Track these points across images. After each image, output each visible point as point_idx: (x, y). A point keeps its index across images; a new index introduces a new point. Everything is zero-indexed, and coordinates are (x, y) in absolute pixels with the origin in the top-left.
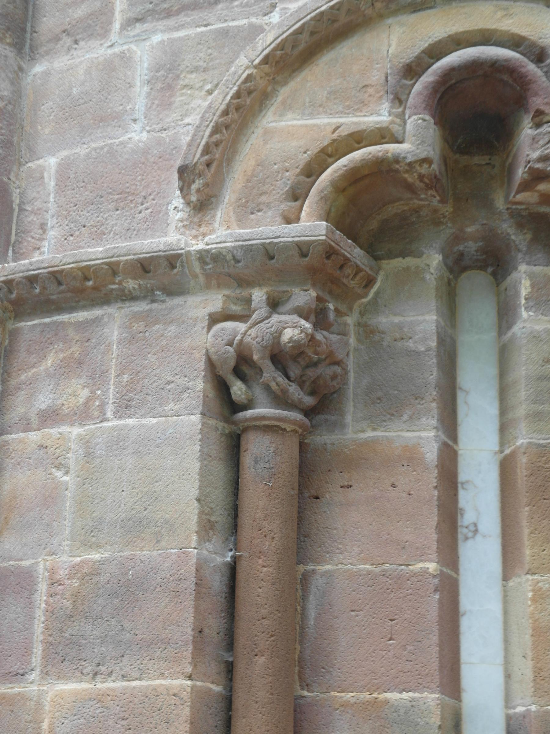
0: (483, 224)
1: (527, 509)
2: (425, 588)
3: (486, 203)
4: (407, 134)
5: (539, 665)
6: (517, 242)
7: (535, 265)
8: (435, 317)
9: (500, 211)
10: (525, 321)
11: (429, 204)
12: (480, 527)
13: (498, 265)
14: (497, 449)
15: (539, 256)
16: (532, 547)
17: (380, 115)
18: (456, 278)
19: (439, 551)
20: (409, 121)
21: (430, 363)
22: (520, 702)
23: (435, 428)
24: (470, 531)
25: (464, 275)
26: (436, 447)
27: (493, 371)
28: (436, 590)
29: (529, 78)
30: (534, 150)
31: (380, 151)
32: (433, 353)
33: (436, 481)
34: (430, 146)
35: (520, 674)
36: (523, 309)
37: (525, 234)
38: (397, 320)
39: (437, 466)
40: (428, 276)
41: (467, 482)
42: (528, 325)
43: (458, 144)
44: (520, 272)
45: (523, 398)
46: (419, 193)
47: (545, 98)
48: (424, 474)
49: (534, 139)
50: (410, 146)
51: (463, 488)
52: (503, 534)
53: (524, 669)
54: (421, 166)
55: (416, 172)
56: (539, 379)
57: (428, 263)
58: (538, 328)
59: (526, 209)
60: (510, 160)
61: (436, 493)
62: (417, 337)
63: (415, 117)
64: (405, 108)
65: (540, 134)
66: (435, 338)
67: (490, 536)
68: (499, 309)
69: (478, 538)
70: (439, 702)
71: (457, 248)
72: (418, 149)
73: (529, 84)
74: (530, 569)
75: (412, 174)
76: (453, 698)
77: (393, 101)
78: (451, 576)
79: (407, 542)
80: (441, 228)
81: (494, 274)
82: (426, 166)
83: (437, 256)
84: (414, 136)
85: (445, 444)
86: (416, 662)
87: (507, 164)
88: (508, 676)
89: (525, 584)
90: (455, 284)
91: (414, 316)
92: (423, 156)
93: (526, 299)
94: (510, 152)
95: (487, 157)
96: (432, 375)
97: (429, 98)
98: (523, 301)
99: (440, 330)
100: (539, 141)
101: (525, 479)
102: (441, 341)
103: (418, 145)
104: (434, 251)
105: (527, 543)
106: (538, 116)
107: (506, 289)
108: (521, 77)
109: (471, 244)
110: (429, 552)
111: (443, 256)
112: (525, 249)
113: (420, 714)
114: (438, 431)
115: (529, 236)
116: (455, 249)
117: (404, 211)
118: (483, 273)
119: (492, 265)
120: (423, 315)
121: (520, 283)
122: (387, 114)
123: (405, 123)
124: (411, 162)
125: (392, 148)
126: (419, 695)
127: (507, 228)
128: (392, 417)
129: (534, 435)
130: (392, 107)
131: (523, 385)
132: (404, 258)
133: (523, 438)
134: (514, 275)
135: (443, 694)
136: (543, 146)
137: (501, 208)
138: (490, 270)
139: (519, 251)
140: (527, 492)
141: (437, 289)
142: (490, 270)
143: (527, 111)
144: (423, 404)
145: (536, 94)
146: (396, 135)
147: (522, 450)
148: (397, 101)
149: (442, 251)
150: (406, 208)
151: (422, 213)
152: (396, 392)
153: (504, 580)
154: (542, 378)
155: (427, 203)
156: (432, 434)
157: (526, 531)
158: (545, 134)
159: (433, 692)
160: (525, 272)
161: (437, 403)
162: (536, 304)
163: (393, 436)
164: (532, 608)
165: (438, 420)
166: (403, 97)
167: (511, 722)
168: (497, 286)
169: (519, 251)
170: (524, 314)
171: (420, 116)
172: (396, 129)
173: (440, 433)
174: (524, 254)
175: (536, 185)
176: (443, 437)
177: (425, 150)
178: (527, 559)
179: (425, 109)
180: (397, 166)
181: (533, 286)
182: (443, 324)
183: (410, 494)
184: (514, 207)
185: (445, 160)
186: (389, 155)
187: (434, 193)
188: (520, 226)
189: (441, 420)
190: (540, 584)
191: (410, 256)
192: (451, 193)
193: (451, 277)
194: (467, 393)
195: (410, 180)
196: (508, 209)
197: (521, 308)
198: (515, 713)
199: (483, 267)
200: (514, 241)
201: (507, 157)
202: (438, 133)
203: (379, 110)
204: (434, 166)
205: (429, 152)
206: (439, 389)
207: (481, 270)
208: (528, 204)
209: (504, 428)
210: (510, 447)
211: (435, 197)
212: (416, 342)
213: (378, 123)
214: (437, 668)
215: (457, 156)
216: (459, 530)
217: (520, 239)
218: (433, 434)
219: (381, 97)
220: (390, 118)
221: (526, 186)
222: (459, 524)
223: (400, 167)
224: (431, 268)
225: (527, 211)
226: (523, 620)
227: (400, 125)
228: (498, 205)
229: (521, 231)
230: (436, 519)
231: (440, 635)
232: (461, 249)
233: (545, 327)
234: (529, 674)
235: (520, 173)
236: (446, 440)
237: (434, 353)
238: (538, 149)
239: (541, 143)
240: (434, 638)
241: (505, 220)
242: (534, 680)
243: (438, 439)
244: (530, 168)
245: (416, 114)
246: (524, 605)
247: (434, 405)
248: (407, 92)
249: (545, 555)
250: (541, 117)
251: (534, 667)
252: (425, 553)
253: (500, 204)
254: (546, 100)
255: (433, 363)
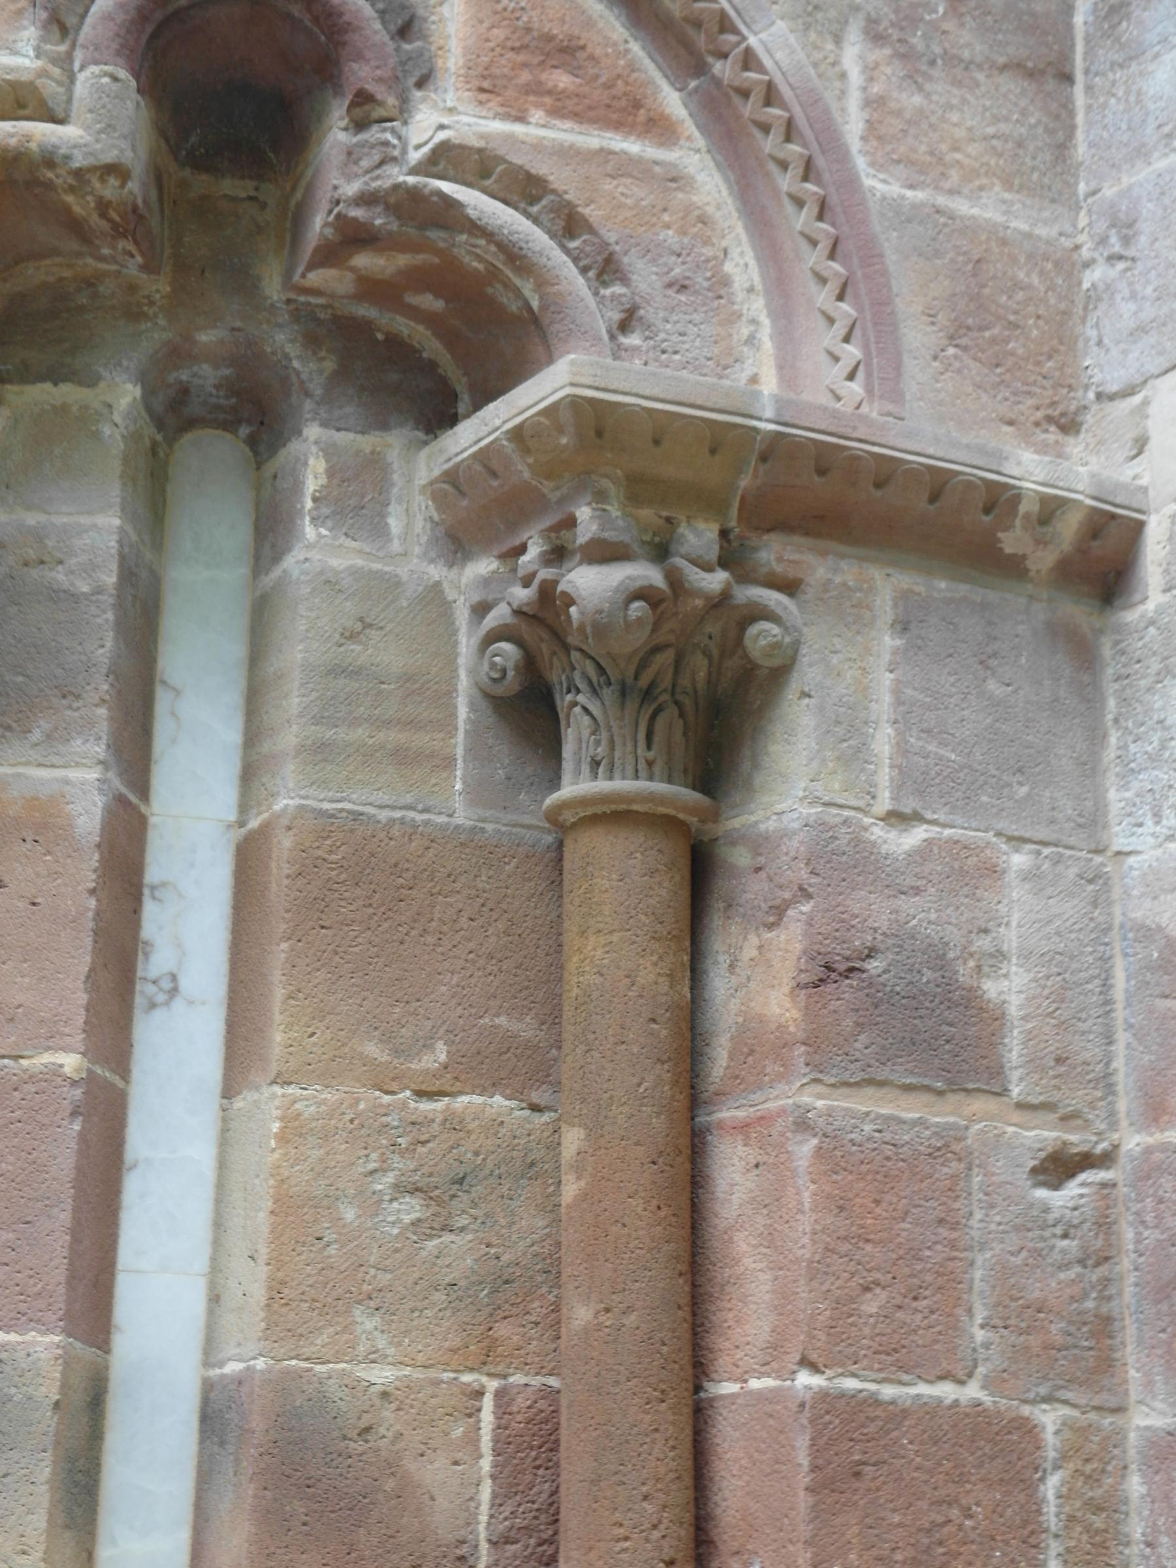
0: (233, 329)
1: (284, 946)
2: (52, 1108)
3: (244, 284)
4: (75, 104)
5: (280, 1274)
6: (304, 376)
7: (338, 430)
8: (117, 522)
9: (272, 305)
10: (310, 547)
11: (119, 272)
12: (184, 983)
13: (262, 423)
14: (233, 817)
15: (349, 409)
16: (289, 1026)
17: (15, 52)
18: (171, 441)
19: (89, 1028)
20: (81, 77)
21: (99, 620)
22: (233, 1351)
23: (101, 762)
24: (161, 989)
25: (188, 437)
26: (100, 804)
27: (236, 650)
28: (74, 1114)
29: (346, 18)
30: (349, 178)
31: (12, 135)
32: (108, 600)
33: (94, 877)
34: (125, 138)
35: (240, 1294)
36: (307, 519)
37: (323, 359)
38: (32, 519)
39: (98, 846)
40: (107, 430)
41: (164, 885)
42: (315, 555)
43: (189, 146)
44: (305, 440)
45: (295, 711)
46: (97, 242)
47: (378, 67)
48: (69, 861)
49: (350, 153)
50: (80, 132)
51: (154, 898)
52: (230, 998)
53: (250, 1282)
54: (102, 180)
55: (91, 193)
56: (329, 672)
57: (108, 399)
58: (337, 563)
59: (325, 307)
60: (299, 195)
61: (93, 903)
62: (74, 561)
63: (96, 69)
64: (73, 46)
65: (363, 146)
66: (114, 566)
67: (203, 1003)
68: (257, 519)
69: (178, 1005)
70: (60, 1351)
71: (175, 375)
72: (97, 141)
73: (346, 32)
74: (279, 1074)
75: (83, 197)
76: (91, 1345)
77: (45, 27)
78: (113, 1085)
79: (20, 1006)
80: (143, 327)
81: (252, 442)
82: (113, 181)
83: (129, 386)
84: (91, 111)
85: (121, 800)
86: (17, 1267)
87: (293, 202)
88: (215, 1299)
89: (267, 1104)
90: (167, 455)
91: (71, 514)
92: (109, 157)
93: (315, 500)
94: (298, 179)
95: (250, 183)
96: (103, 647)
97: (128, 31)
98: (309, 504)
99: (126, 550)
100: (360, 159)
101: (286, 882)
102: (128, 575)
103: (99, 132)
104: (125, 377)
105: (278, 1018)
106: (359, 105)
107: (275, 477)
108: (330, 15)
109: (206, 369)
110: (67, 1030)
111: (143, 388)
112: (319, 392)
113: (17, 1379)
114: (107, 769)
115: (330, 365)
116: (171, 378)
117: (61, 279)
118: (228, 436)
119: (249, 422)
120: (90, 513)
121: (306, 464)
122: (32, 53)
123: (72, 79)
124: (80, 169)
125: (40, 132)
126: (19, 1338)
127: (283, 341)
128: (8, 734)
129: (311, 791)
130: (43, 39)
131: (297, 684)
132: (56, 384)
133: (287, 797)
134: (295, 447)
135: (70, 1335)
136: (367, 172)
137: (275, 298)
138: (244, 431)
139: (308, 394)
140: (288, 911)
141: (126, 460)
142: (244, 431)
143: (338, 91)
144: (78, 709)
145: (359, 57)
146: (50, 104)
147: (285, 822)
148: (55, 28)
149: (142, 378)
150: (67, 274)
151: (101, 289)
152: (20, 679)
153: (224, 1097)
154: (337, 671)
155: (114, 267)
156: (93, 775)
157: (279, 993)
158: (373, 146)
159: (49, 1331)
160: (316, 443)
161: (109, 709)
162: (334, 513)
163: (7, 775)
164: (276, 1155)
165: (108, 746)
166: (71, 21)
167: (212, 1395)
168: (258, 469)
169: (308, 394)
170: (310, 531)
171: (106, 68)
172: (50, 89)
173: (110, 775)
174: (318, 403)
175: (351, 256)
176: (118, 785)
177: (114, 146)
178: (277, 1051)
179: (118, 53)
180: (50, 175)
181: (331, 473)
182: (134, 537)
183: (34, 904)
184: (302, 299)
185: (158, 177)
186: (33, 146)
187: (131, 247)
188: (312, 341)
189: (117, 747)
190: (297, 1106)
191: (70, 380)
192: (168, 252)
193: (159, 438)
194: (178, 692)
195: (77, 209)
196: (289, 301)
197: (302, 519)
198: (223, 1376)
199: (229, 425)
200: (298, 374)
201: (294, 189)
202: (144, 113)
203: (15, 41)
204: (133, 186)
205: (122, 151)
206: (117, 679)
207: (225, 429)
208: (332, 296)
209: (251, 774)
210: (260, 813)
211: (132, 256)
212: (72, 572)
213: (11, 70)
214: (62, 1279)
215: (187, 172)
216: (138, 987)
217: (309, 369)
218: (96, 776)
219: (19, 13)
220: (39, 63)
221: (328, 255)
222: (139, 974)
223: (57, 176)
224: (115, 413)
225: (329, 311)
226: (257, 1181)
227: (60, 83)
228: (267, 292)
229: (314, 353)
230: (88, 959)
231: (76, 1210)
232: (184, 378)
233: (351, 562)
234: (259, 1293)
235: (318, 225)
236: (124, 790)
237: (111, 600)
238: (357, 175)
239: (365, 163)
240: (62, 1216)
241: (280, 326)
242: (268, 1305)
243: (105, 787)
244: (339, 216)
245: (96, 63)
246: (262, 1153)
247: (102, 711)
248: (80, 10)
249: (315, 1044)
250: (366, 107)
251: (271, 1278)
252: (58, 1032)
253: (273, 289)
254: (378, 72)
255: (107, 620)
